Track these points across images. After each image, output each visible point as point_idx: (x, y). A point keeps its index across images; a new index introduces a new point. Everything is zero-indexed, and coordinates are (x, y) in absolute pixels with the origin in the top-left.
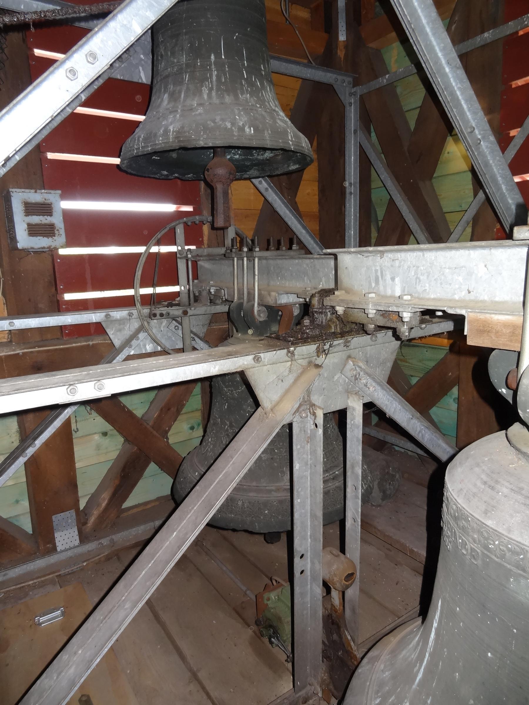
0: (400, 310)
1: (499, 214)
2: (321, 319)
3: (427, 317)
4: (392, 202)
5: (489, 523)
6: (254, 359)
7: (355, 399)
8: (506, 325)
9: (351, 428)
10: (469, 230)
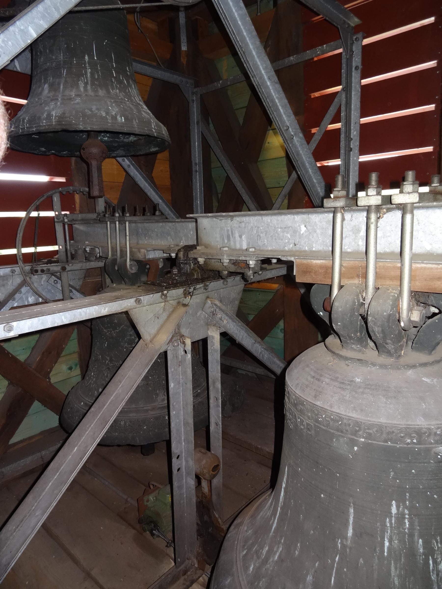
0: (247, 259)
1: (308, 190)
2: (187, 268)
3: (265, 266)
4: (228, 178)
5: (318, 403)
6: (136, 301)
7: (214, 330)
8: (321, 266)
9: (211, 353)
10: (286, 201)
